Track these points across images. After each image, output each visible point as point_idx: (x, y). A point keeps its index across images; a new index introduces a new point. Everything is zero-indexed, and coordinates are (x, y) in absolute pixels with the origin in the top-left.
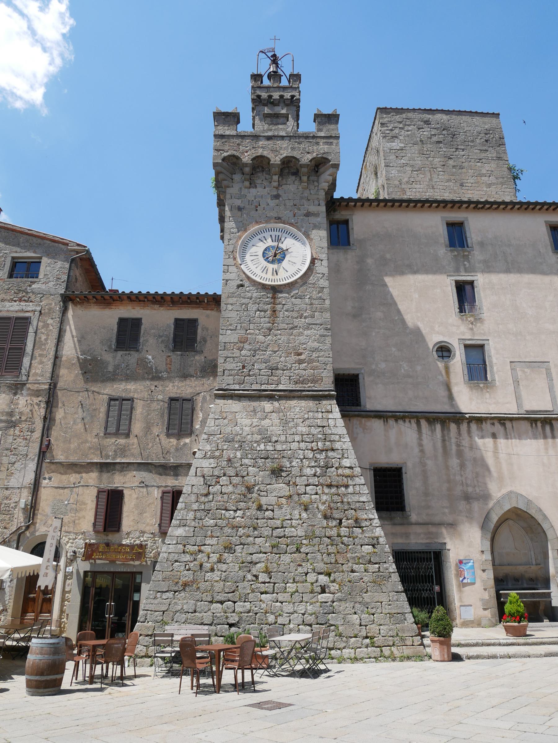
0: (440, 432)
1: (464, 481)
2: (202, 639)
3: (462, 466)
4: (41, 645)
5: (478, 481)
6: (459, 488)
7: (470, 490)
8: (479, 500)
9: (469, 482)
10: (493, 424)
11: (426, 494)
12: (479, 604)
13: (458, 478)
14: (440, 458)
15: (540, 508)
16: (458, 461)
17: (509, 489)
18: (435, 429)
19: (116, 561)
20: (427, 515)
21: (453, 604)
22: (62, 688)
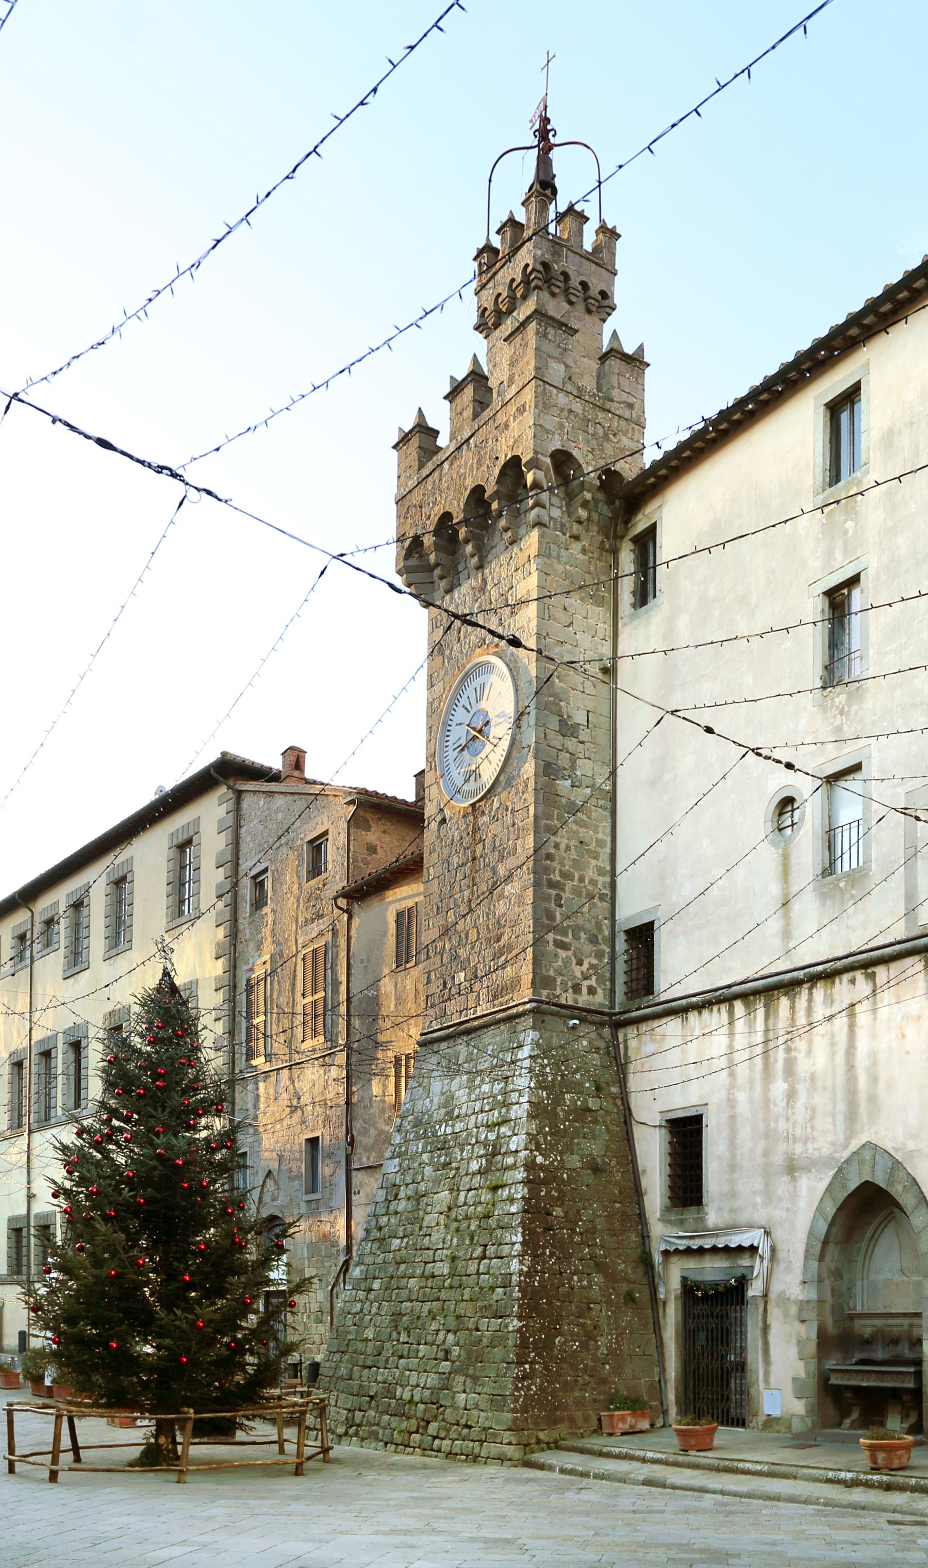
0: (763, 1021)
1: (791, 1131)
2: (224, 1414)
3: (791, 1095)
4: (596, 1442)
5: (813, 1128)
6: (782, 1147)
7: (798, 1149)
8: (810, 1171)
9: (798, 1132)
10: (853, 981)
11: (733, 1167)
12: (788, 1387)
13: (782, 1125)
14: (758, 1086)
15: (914, 1179)
16: (785, 1086)
17: (863, 1138)
18: (755, 1018)
19: (599, 487)
20: (732, 1210)
21: (756, 1386)
22: (411, 797)
